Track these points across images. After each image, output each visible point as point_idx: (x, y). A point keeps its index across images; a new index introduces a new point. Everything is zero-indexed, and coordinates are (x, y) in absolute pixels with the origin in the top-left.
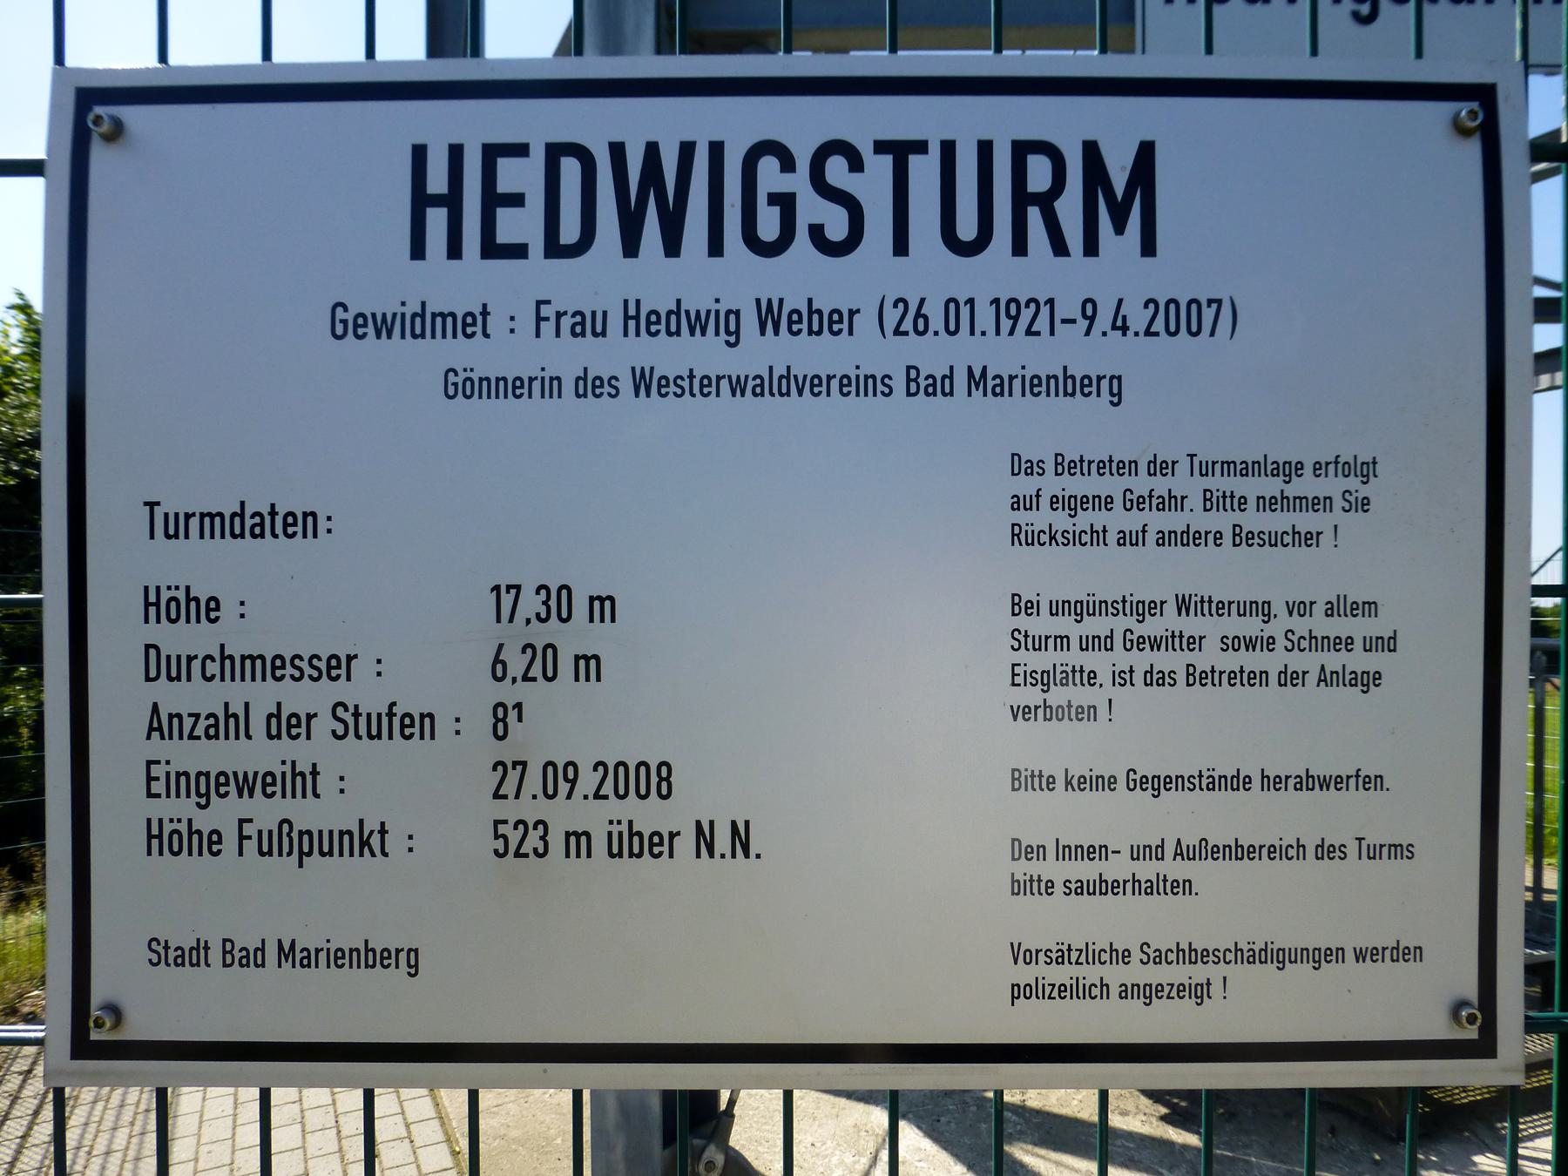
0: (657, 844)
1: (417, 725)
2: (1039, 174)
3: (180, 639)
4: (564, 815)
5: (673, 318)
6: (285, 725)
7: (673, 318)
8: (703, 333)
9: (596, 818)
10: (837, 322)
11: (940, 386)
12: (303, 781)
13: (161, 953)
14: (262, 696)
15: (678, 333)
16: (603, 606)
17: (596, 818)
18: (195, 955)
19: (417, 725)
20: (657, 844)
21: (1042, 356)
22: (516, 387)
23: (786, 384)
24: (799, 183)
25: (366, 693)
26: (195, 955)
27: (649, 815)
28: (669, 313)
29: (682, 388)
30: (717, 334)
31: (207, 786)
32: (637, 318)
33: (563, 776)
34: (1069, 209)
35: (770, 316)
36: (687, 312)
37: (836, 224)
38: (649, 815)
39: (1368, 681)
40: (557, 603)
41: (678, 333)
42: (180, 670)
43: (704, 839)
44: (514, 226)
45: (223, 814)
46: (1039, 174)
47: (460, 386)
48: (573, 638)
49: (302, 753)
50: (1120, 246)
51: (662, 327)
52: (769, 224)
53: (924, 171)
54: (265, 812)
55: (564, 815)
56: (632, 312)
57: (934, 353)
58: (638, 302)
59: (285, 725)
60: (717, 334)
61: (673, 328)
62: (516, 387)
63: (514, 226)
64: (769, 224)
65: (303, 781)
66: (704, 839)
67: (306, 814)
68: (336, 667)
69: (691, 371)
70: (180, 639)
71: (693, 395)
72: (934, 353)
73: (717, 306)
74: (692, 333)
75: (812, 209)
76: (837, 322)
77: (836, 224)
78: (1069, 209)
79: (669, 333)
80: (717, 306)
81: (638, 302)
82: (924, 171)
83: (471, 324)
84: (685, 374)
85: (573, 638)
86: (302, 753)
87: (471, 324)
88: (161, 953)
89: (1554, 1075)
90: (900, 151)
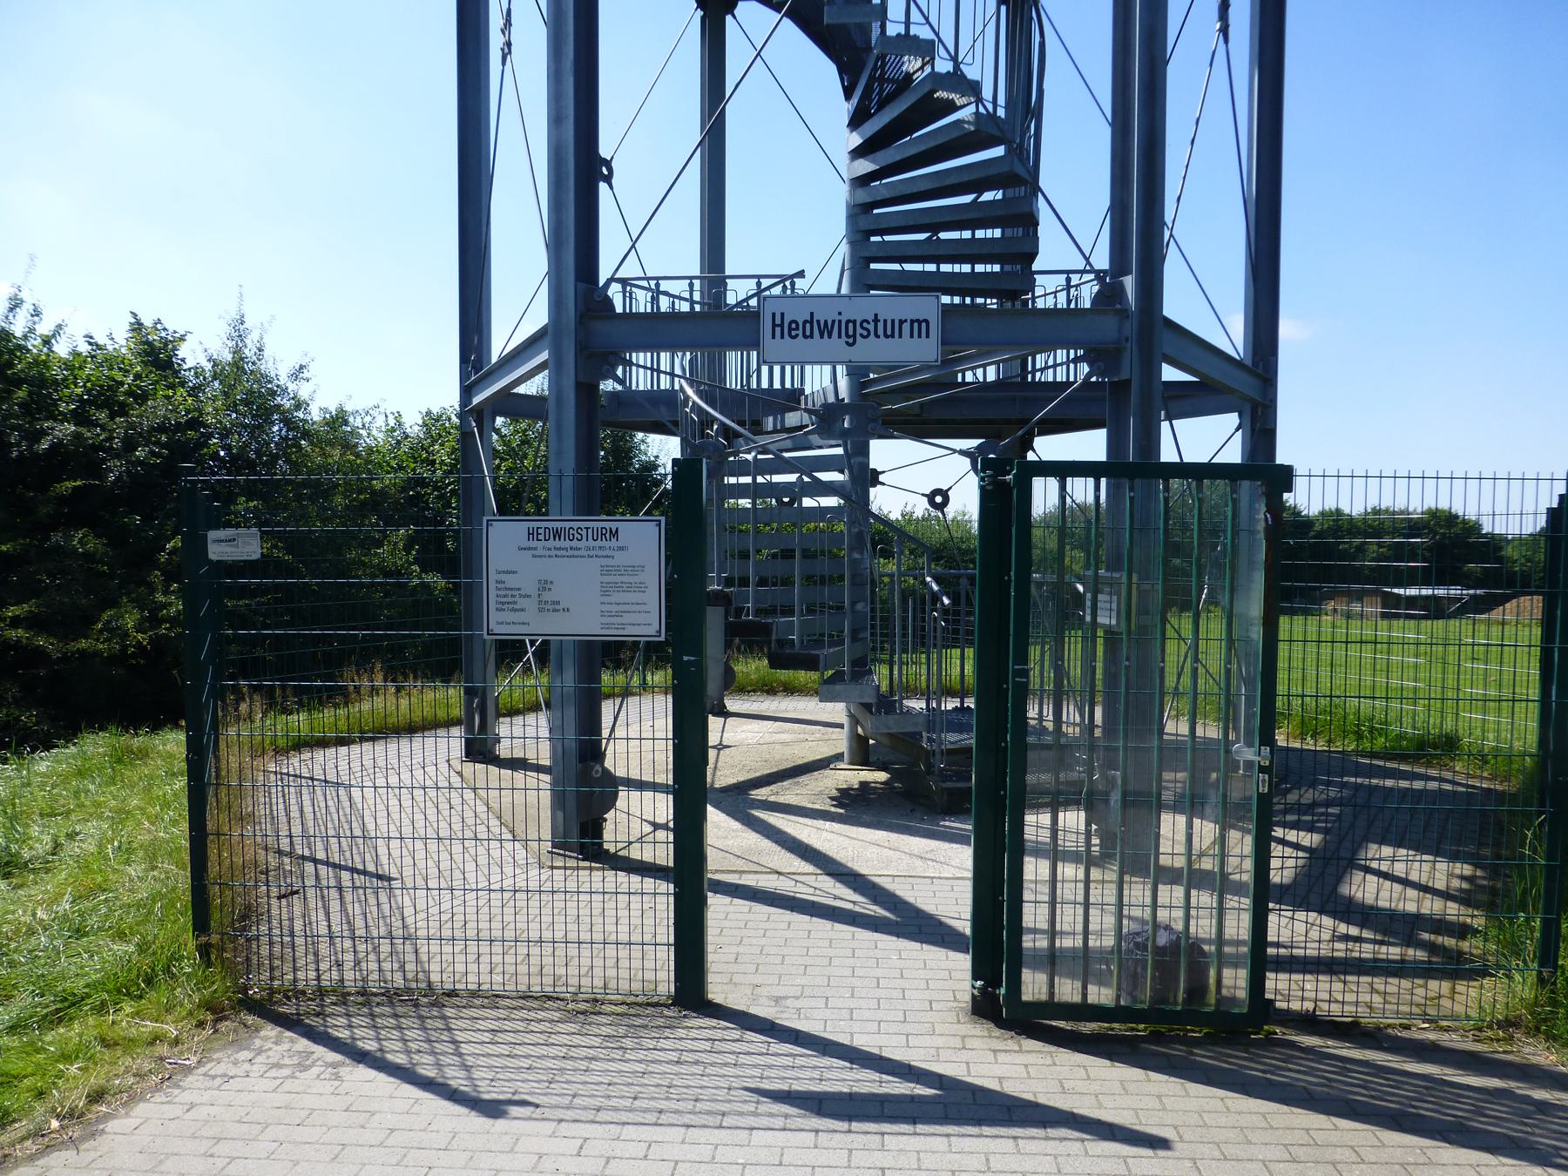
0: (558, 610)
1: (529, 596)
2: (604, 531)
3: (500, 586)
4: (547, 607)
5: (808, 325)
6: (513, 596)
7: (808, 325)
8: (830, 337)
9: (550, 607)
10: (579, 549)
11: (592, 557)
12: (515, 603)
13: (498, 623)
14: (510, 593)
15: (811, 336)
16: (551, 582)
17: (550, 607)
18: (502, 623)
19: (529, 596)
20: (558, 610)
21: (604, 553)
22: (541, 556)
23: (574, 556)
24: (575, 532)
25: (522, 592)
26: (502, 623)
27: (557, 607)
28: (805, 322)
29: (868, 331)
30: (840, 337)
31: (503, 603)
32: (782, 325)
33: (546, 602)
34: (608, 535)
35: (571, 548)
36: (818, 322)
37: (580, 538)
38: (557, 607)
39: (644, 592)
40: (546, 582)
41: (811, 336)
42: (499, 589)
43: (564, 610)
44: (540, 537)
45: (506, 606)
46: (604, 531)
47: (534, 556)
48: (548, 586)
49: (515, 599)
50: (614, 540)
51: (800, 332)
52: (571, 537)
53: (590, 531)
54: (511, 606)
55: (547, 607)
56: (778, 321)
57: (591, 553)
58: (782, 314)
59: (513, 596)
60: (840, 337)
61: (808, 333)
62: (541, 556)
63: (540, 537)
64: (571, 537)
65: (515, 603)
66: (564, 610)
67: (516, 607)
68: (519, 589)
69: (876, 315)
70: (500, 586)
71: (877, 336)
72: (591, 553)
73: (840, 317)
74: (822, 337)
75: (576, 535)
76: (579, 549)
77: (580, 538)
78: (608, 535)
79: (805, 336)
80: (840, 317)
81: (782, 314)
82: (590, 531)
83: (535, 549)
84: (871, 318)
85: (548, 586)
86: (515, 599)
87: (535, 549)
88: (498, 623)
89: (974, 735)
90: (587, 528)
